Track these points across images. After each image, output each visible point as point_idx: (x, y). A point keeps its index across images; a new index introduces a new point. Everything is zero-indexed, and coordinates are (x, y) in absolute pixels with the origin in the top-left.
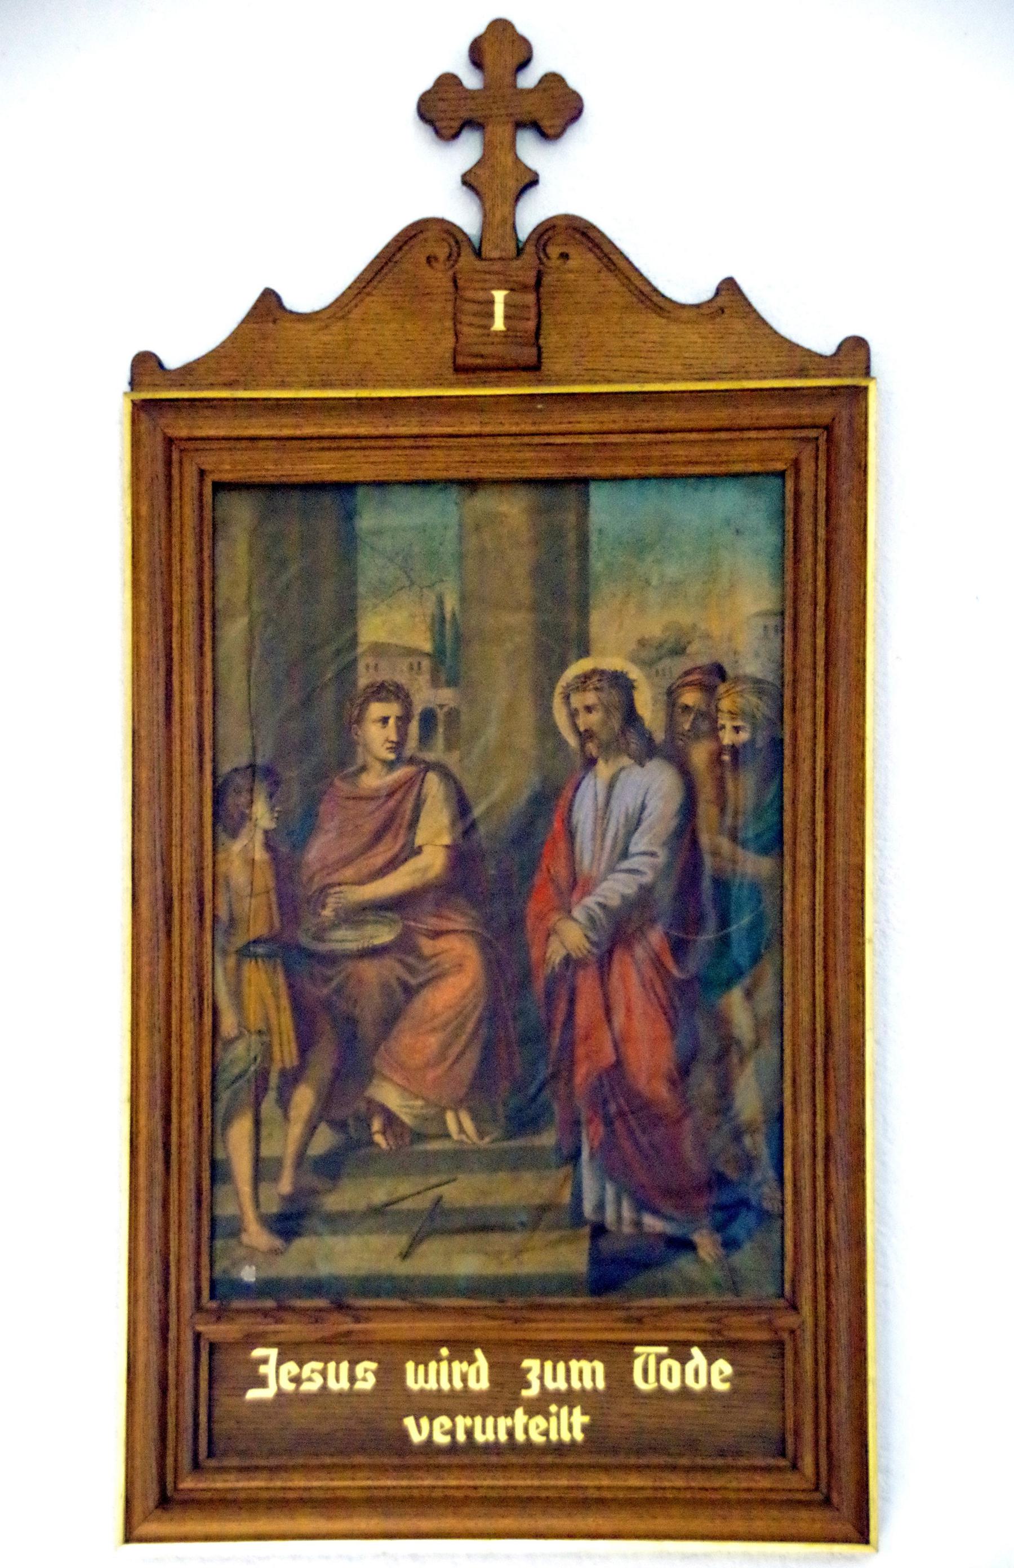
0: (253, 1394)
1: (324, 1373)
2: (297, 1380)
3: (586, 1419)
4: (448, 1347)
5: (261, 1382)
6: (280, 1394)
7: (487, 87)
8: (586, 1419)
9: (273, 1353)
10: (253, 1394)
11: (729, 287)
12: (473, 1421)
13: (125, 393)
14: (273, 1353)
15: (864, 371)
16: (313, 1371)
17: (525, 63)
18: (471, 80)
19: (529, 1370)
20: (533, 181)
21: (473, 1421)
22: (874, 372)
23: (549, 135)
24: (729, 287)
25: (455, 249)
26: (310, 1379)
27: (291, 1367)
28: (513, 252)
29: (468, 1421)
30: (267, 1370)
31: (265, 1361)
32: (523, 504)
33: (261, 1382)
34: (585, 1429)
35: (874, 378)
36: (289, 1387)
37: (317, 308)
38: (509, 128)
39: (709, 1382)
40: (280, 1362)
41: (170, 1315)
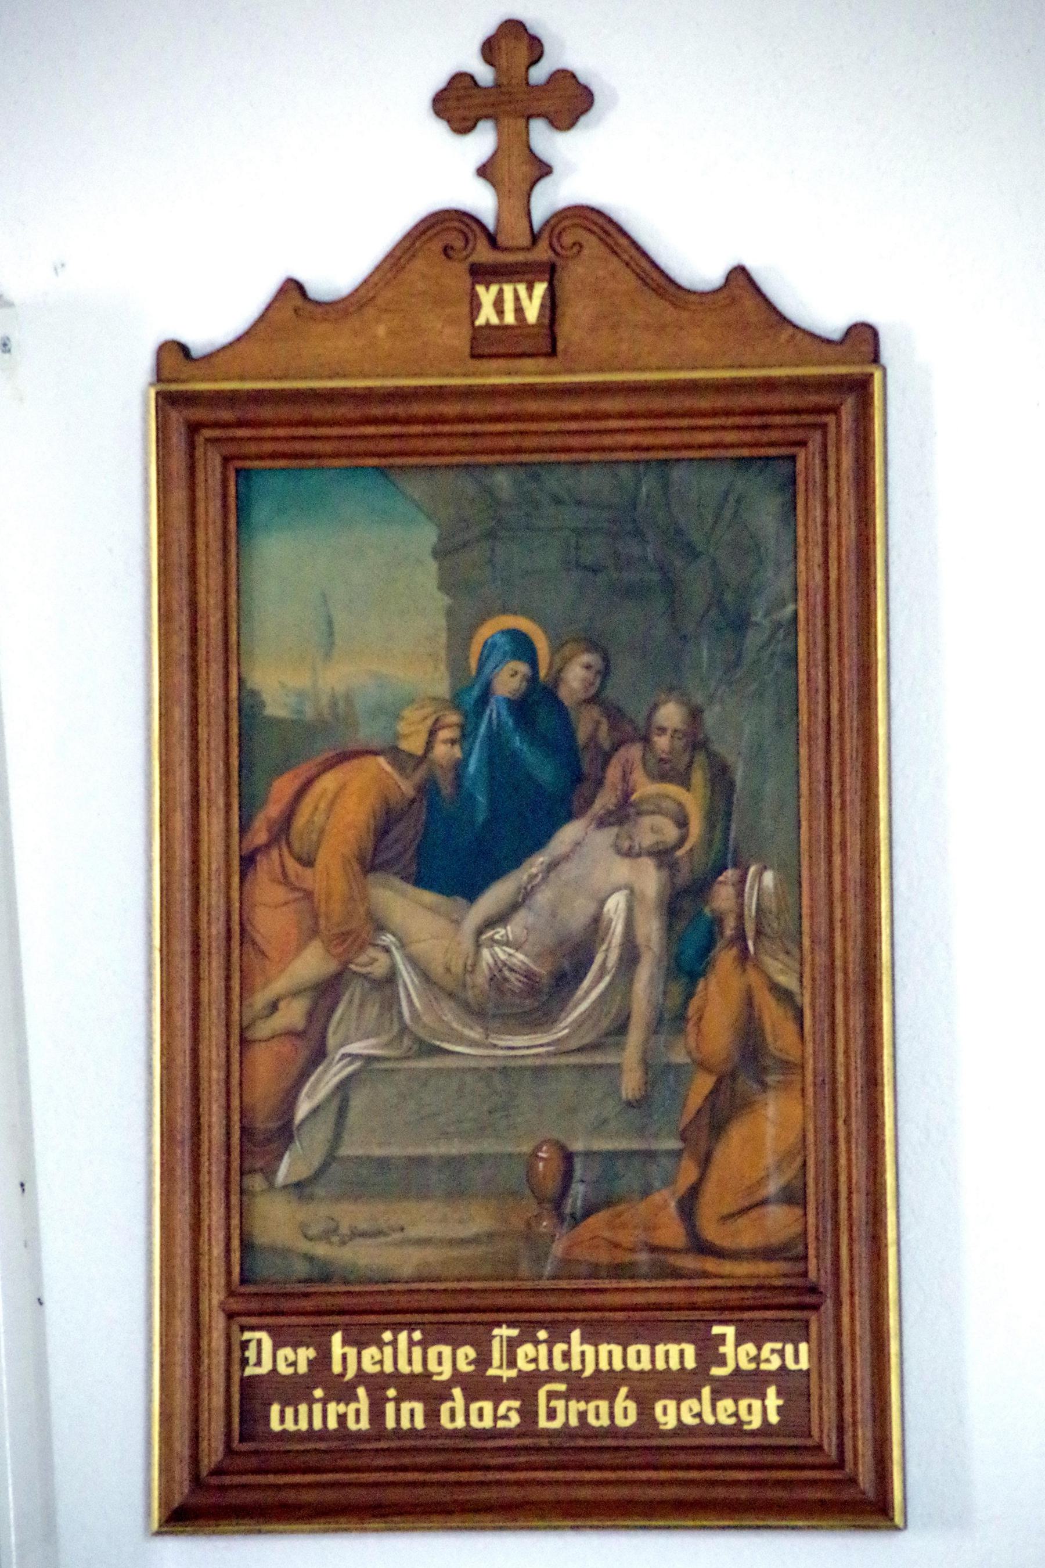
1: (782, 1353)
2: (756, 1359)
3: (780, 1402)
5: (722, 1361)
6: (737, 1371)
7: (497, 85)
8: (780, 1402)
9: (730, 1331)
11: (740, 275)
14: (730, 1331)
15: (872, 356)
17: (536, 60)
18: (484, 74)
20: (484, 172)
24: (740, 275)
25: (555, 240)
26: (767, 1361)
27: (750, 1348)
28: (525, 241)
30: (727, 1349)
31: (722, 1338)
33: (722, 1361)
34: (780, 1410)
36: (746, 1366)
38: (523, 121)
39: (359, 1353)
40: (738, 1344)
41: (413, 1288)
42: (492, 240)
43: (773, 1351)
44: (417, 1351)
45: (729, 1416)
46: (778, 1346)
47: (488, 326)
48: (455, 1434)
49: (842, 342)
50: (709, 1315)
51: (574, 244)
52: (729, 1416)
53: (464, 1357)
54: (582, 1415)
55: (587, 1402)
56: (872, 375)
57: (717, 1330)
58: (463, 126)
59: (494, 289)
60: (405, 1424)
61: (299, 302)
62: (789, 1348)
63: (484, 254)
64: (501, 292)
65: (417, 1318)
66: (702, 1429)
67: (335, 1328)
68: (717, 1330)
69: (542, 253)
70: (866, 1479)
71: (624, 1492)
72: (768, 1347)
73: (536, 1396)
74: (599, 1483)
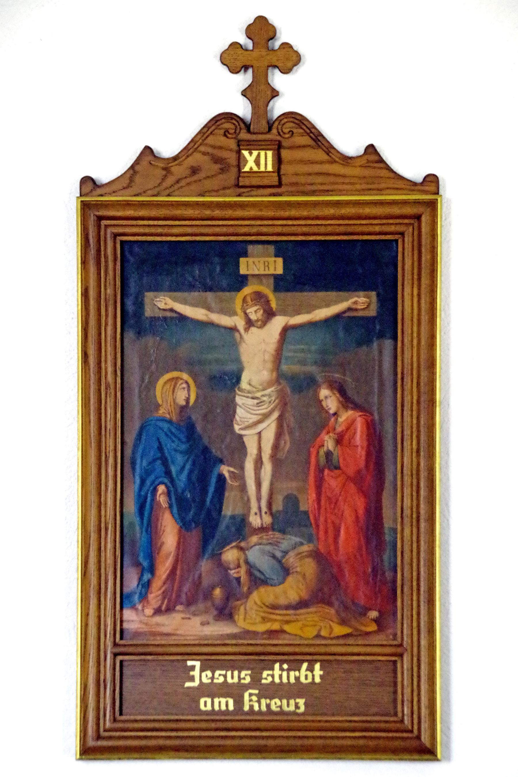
0: (188, 684)
1: (225, 676)
4: (287, 664)
5: (192, 679)
10: (188, 684)
11: (371, 149)
12: (281, 702)
13: (77, 197)
14: (197, 664)
16: (246, 675)
19: (193, 668)
21: (281, 702)
22: (441, 192)
23: (286, 71)
24: (371, 149)
29: (268, 701)
31: (193, 668)
32: (131, 331)
33: (192, 679)
35: (441, 195)
37: (176, 153)
40: (202, 670)
42: (248, 127)
43: (268, 675)
44: (285, 674)
45: (277, 707)
46: (223, 672)
47: (251, 172)
48: (207, 713)
49: (422, 184)
50: (186, 657)
51: (290, 131)
52: (277, 707)
53: (205, 676)
54: (268, 706)
55: (271, 700)
56: (437, 200)
57: (190, 663)
58: (234, 71)
59: (255, 153)
60: (223, 708)
61: (151, 158)
62: (229, 673)
63: (244, 135)
64: (259, 156)
65: (286, 657)
66: (282, 713)
67: (316, 661)
68: (190, 663)
69: (273, 135)
70: (425, 738)
71: (177, 742)
72: (217, 673)
73: (242, 697)
74: (241, 737)
